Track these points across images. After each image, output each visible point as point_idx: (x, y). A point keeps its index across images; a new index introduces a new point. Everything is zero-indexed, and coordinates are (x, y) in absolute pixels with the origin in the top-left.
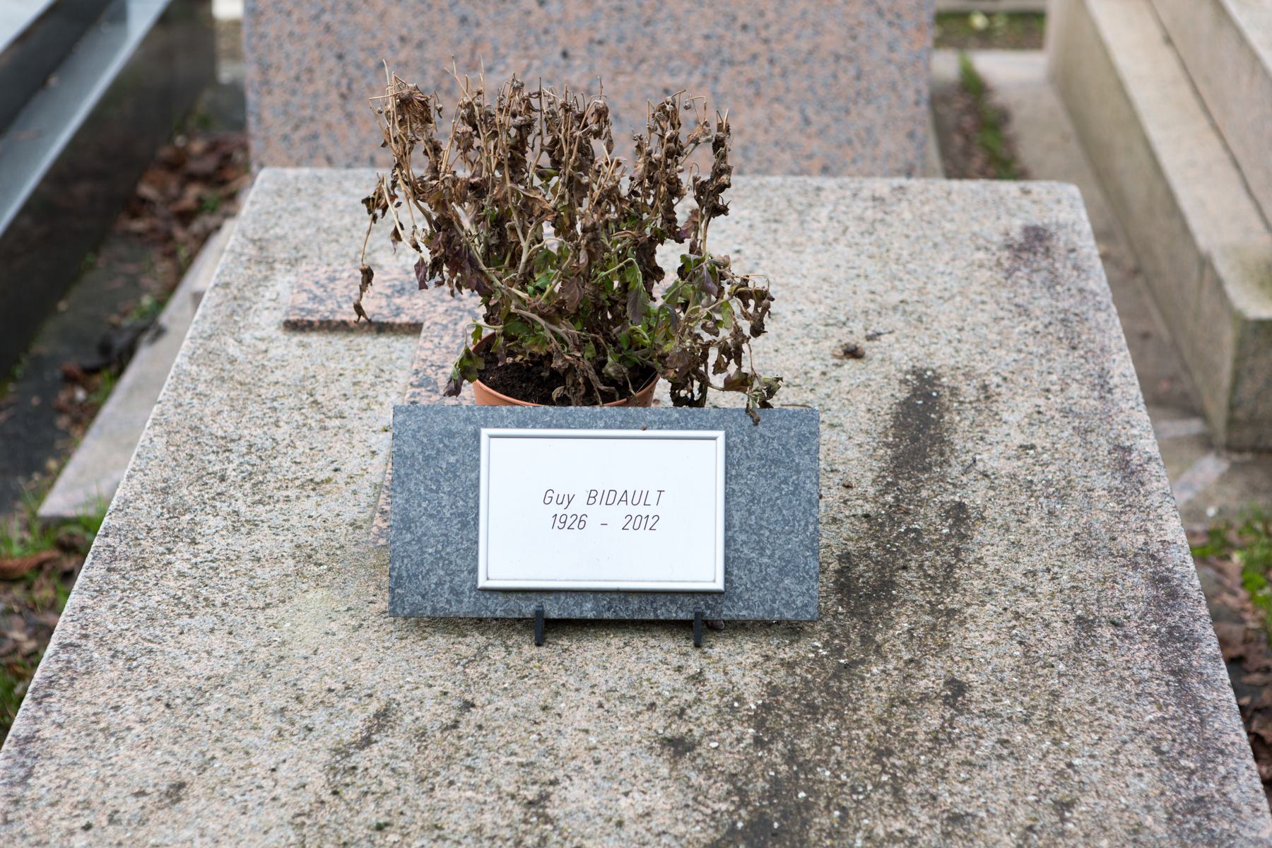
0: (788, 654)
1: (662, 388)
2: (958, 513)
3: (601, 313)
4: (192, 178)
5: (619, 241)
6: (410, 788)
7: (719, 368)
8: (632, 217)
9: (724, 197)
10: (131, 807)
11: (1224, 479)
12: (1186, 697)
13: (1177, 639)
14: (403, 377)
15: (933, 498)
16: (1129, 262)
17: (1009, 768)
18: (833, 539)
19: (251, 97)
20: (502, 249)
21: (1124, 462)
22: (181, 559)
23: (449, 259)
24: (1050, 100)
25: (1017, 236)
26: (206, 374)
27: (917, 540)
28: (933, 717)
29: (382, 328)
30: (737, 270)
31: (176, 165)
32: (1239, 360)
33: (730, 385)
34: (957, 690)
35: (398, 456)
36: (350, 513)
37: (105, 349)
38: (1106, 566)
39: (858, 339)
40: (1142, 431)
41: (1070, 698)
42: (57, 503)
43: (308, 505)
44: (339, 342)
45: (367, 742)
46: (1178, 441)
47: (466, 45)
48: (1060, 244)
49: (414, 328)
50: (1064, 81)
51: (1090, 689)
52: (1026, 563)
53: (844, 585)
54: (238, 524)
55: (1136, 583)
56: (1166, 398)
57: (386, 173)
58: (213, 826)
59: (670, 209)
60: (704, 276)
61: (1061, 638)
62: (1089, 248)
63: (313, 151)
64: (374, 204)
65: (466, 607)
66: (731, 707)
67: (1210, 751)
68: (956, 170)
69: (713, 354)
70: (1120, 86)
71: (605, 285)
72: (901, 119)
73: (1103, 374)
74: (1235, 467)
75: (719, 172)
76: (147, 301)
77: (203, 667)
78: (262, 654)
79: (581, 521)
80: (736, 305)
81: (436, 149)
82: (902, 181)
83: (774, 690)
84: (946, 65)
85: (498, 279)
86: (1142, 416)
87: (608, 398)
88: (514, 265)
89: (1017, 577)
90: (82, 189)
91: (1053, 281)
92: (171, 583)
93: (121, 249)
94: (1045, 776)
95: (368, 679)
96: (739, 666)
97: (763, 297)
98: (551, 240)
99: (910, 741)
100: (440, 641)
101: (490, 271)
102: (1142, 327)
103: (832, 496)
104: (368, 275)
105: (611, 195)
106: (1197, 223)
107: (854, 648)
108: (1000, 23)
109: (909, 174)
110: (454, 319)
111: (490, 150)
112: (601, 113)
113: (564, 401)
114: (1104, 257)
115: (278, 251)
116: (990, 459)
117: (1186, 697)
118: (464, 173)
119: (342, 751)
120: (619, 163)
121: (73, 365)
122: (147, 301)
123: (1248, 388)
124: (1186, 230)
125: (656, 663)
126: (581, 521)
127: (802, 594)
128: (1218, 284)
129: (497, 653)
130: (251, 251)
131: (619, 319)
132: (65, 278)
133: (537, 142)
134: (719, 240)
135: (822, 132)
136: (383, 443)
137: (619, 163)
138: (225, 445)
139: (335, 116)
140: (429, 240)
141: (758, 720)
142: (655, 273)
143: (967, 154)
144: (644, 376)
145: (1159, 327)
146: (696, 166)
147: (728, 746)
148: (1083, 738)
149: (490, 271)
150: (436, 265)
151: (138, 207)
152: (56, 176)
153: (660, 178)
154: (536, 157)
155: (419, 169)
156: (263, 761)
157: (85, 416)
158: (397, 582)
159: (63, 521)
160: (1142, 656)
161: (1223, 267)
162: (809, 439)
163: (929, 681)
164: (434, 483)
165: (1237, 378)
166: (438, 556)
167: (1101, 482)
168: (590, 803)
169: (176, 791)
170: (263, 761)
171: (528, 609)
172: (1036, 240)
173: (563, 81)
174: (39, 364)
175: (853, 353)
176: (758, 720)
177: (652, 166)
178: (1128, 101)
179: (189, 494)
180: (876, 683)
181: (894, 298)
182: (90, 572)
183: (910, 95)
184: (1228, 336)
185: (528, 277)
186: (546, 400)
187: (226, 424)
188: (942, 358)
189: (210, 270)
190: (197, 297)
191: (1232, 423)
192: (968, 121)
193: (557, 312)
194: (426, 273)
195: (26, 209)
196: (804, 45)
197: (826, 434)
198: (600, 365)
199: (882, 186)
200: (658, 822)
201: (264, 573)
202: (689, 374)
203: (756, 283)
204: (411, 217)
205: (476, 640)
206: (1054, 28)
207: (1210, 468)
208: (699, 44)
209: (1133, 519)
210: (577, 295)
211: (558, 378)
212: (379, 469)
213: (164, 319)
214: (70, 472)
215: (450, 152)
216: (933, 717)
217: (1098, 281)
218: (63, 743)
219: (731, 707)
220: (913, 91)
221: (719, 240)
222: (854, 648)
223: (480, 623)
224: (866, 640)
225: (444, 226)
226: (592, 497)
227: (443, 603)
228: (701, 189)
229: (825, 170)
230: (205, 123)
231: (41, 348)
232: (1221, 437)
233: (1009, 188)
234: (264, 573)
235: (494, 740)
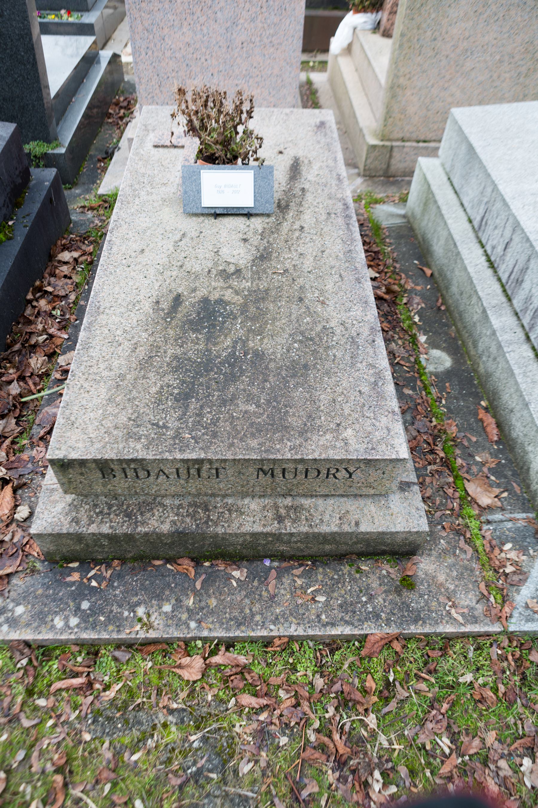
0: (267, 221)
1: (240, 161)
2: (303, 190)
3: (226, 142)
4: (121, 108)
5: (229, 125)
6: (191, 249)
7: (252, 156)
8: (232, 119)
9: (253, 114)
10: (134, 254)
11: (362, 183)
12: (349, 229)
13: (348, 217)
14: (181, 159)
15: (298, 186)
16: (344, 130)
17: (312, 244)
18: (277, 196)
19: (137, 86)
20: (204, 127)
21: (339, 178)
22: (137, 201)
23: (192, 129)
24: (328, 87)
25: (318, 123)
26: (137, 158)
27: (294, 196)
28: (297, 234)
29: (175, 147)
30: (255, 133)
31: (117, 104)
32: (367, 154)
33: (254, 160)
34: (302, 228)
35: (183, 177)
36: (173, 190)
37: (107, 153)
38: (334, 201)
39: (282, 149)
40: (343, 170)
41: (325, 230)
42: (102, 190)
43: (163, 189)
44: (166, 150)
45: (181, 240)
46: (352, 174)
47: (188, 72)
48: (327, 125)
49: (183, 147)
50: (332, 81)
51: (329, 228)
52: (317, 201)
53: (279, 206)
54: (149, 194)
55: (340, 205)
56: (350, 164)
57: (176, 107)
58: (151, 258)
59: (241, 117)
60: (248, 134)
61: (324, 217)
62: (334, 127)
63: (153, 102)
64: (173, 116)
65: (199, 211)
66: (255, 232)
67: (353, 240)
68: (305, 106)
69: (251, 153)
70: (344, 83)
71: (227, 136)
72: (292, 93)
73: (336, 158)
74: (365, 181)
75: (251, 108)
76: (115, 140)
77: (145, 225)
78: (157, 222)
79: (223, 191)
80: (256, 140)
81: (187, 102)
82: (292, 109)
83: (264, 229)
84: (303, 76)
85: (203, 135)
86: (343, 167)
87: (228, 163)
88: (206, 130)
89: (315, 204)
90: (95, 111)
91: (325, 135)
92: (135, 207)
93: (107, 127)
94: (319, 246)
95: (180, 227)
96: (257, 223)
97: (261, 139)
98: (214, 125)
99: (292, 239)
100: (194, 218)
101: (201, 133)
102: (346, 146)
103: (276, 186)
104: (173, 133)
105: (227, 114)
106: (360, 120)
107: (281, 220)
108: (316, 64)
109: (294, 107)
110: (193, 144)
111: (200, 102)
112: (225, 93)
113: (218, 164)
114: (338, 129)
115: (150, 128)
116: (310, 177)
117: (349, 229)
118: (194, 108)
119: (176, 242)
120: (229, 106)
121: (100, 157)
122: (115, 140)
123: (369, 162)
124: (357, 122)
125: (240, 222)
126: (223, 191)
127: (271, 208)
128: (364, 136)
129: (206, 221)
130: (143, 127)
131: (230, 144)
132: (95, 135)
133: (211, 99)
134: (252, 125)
135: (274, 96)
136: (179, 174)
137: (229, 106)
138: (143, 175)
139: (158, 91)
140: (187, 125)
141: (261, 235)
142: (237, 133)
143: (307, 101)
144: (235, 158)
145: (350, 146)
146: (246, 107)
147: (255, 240)
148: (327, 238)
149: (201, 133)
150: (189, 131)
151: (109, 116)
152: (89, 108)
153: (238, 109)
154: (210, 104)
155: (183, 107)
156: (160, 244)
157: (494, 103)
158: (185, 206)
159: (104, 195)
160: (340, 221)
161: (365, 131)
162: (271, 172)
163: (297, 226)
164: (191, 182)
165: (366, 159)
166: (193, 200)
167: (334, 182)
168: (228, 252)
169: (143, 251)
170: (160, 244)
171: (213, 211)
172: (322, 125)
173: (217, 84)
174: (91, 157)
175: (281, 152)
176: (261, 235)
177: (237, 106)
178: (346, 87)
179: (137, 187)
180: (286, 226)
181: (290, 139)
182: (117, 205)
183: (294, 86)
184: (365, 149)
185: (210, 134)
186: (214, 163)
187: (143, 170)
188: (300, 154)
189: (130, 132)
190: (131, 140)
191: (365, 170)
192: (308, 92)
193: (216, 143)
194: (186, 133)
195: (83, 116)
196: (269, 72)
197: (275, 172)
198: (226, 155)
199: (288, 110)
200: (241, 256)
201: (155, 204)
202: (245, 157)
203: (259, 136)
204: (183, 120)
205: (202, 218)
206: (329, 66)
207: (359, 180)
208: (244, 72)
209: (340, 191)
210: (220, 139)
211: (217, 158)
212: (178, 180)
213: (120, 145)
214: (103, 183)
215: (190, 103)
216: (297, 234)
217: (336, 135)
218: (118, 242)
219: (255, 232)
220: (295, 85)
221: (252, 125)
222: (281, 220)
223: (202, 215)
224: (283, 218)
225: (190, 121)
226: (225, 186)
227: (195, 211)
228: (247, 112)
229: (274, 106)
230: (123, 92)
231: (92, 153)
232: (362, 173)
233: (317, 111)
234: (155, 204)
235: (207, 239)
